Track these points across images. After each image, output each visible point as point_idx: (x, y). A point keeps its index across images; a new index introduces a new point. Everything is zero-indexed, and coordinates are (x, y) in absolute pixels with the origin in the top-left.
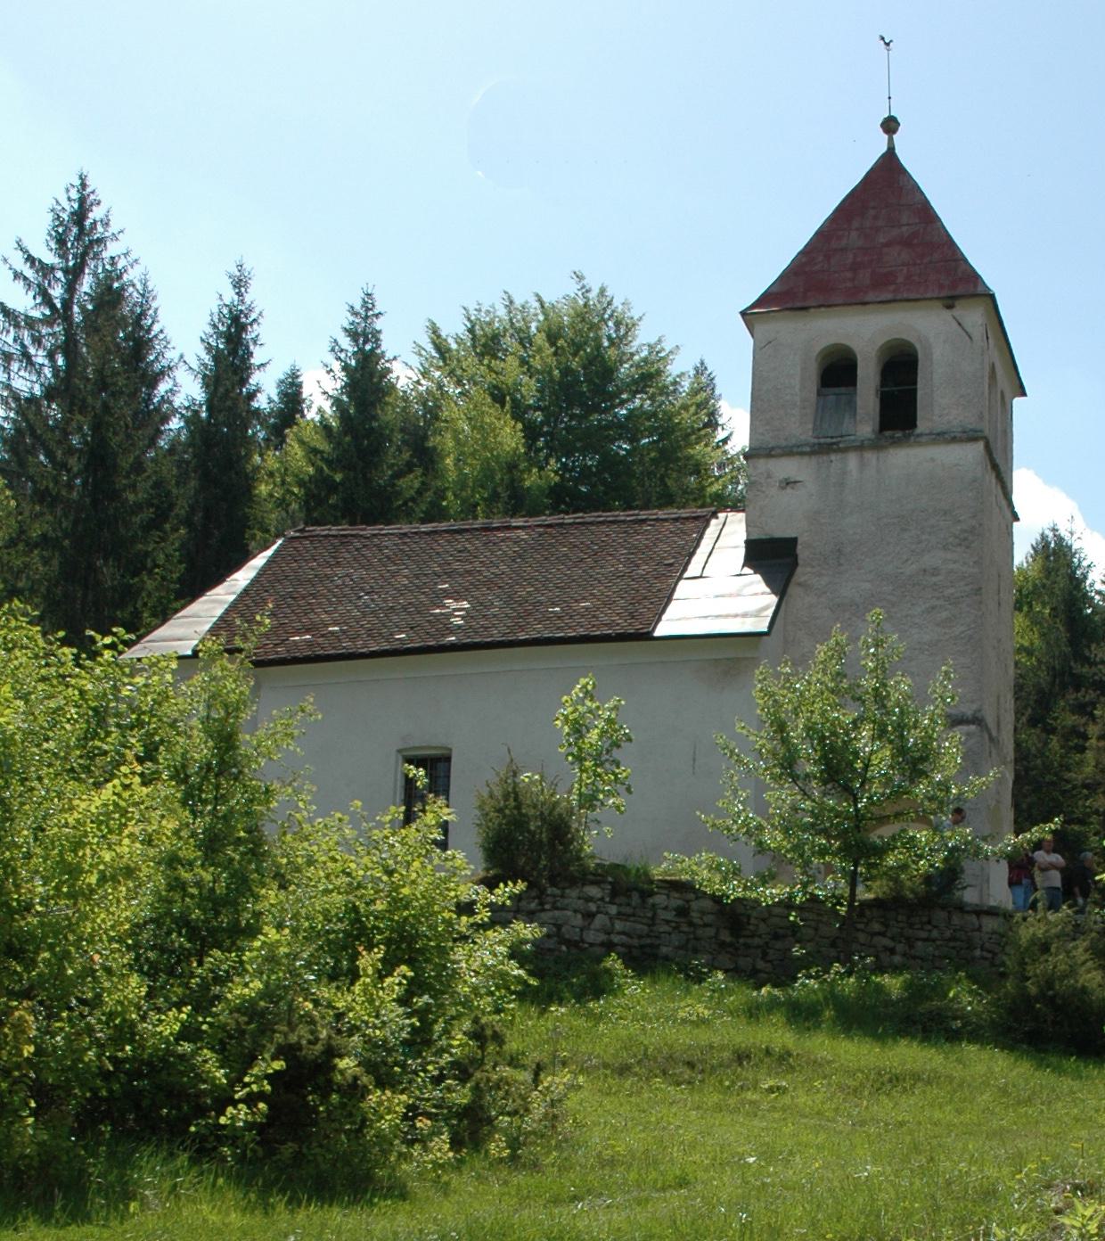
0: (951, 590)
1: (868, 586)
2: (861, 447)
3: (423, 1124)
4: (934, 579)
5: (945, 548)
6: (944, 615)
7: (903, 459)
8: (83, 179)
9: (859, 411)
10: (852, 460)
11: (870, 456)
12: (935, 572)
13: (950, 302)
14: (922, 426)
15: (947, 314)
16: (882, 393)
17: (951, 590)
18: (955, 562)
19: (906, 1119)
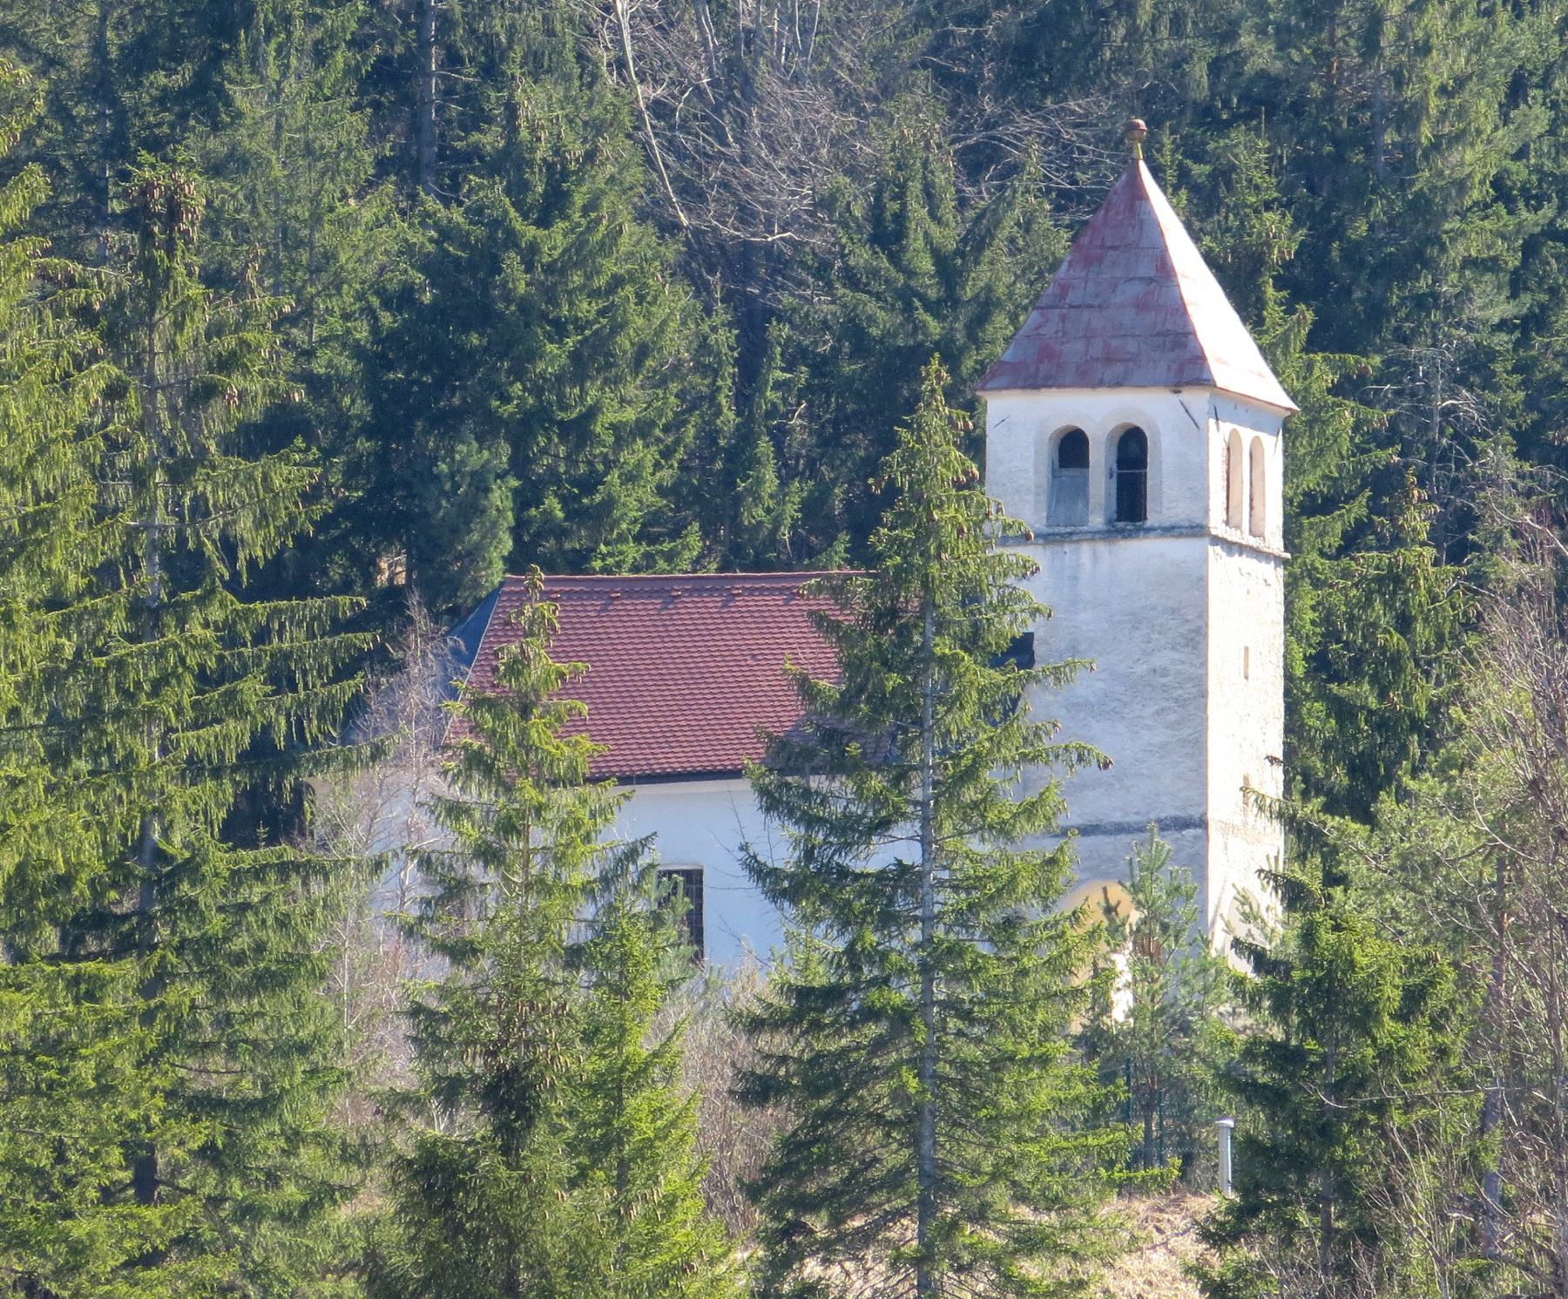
0: (1180, 692)
1: (1100, 685)
2: (1095, 536)
3: (966, 1258)
4: (1164, 680)
5: (1173, 649)
6: (1173, 717)
7: (1137, 552)
8: (1246, 779)
9: (1092, 501)
10: (1086, 548)
11: (1102, 547)
12: (1164, 672)
13: (1177, 386)
14: (1152, 519)
15: (1174, 398)
16: (1120, 476)
17: (1180, 692)
18: (1183, 663)
19: (1299, 1241)
